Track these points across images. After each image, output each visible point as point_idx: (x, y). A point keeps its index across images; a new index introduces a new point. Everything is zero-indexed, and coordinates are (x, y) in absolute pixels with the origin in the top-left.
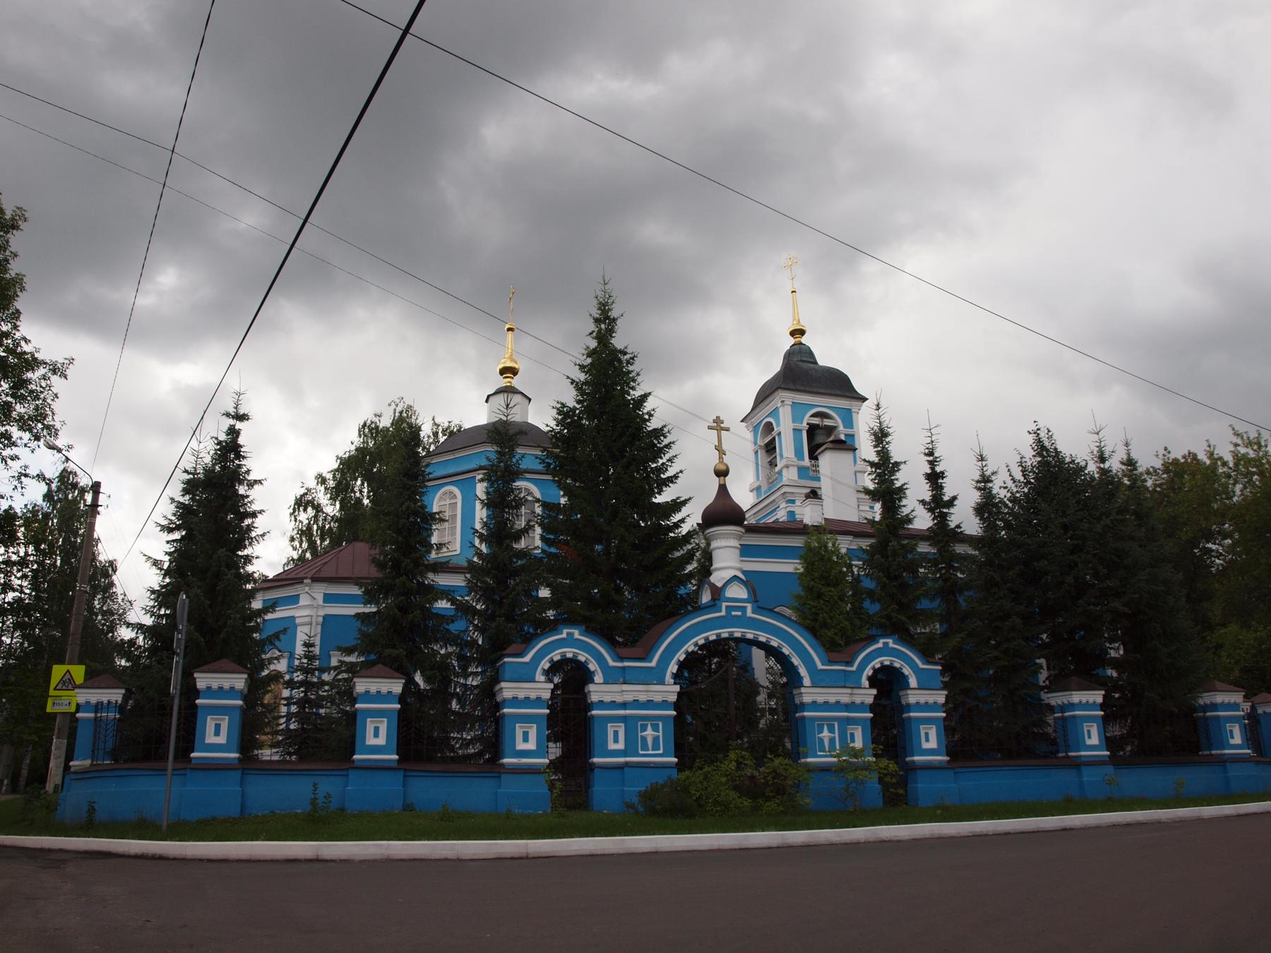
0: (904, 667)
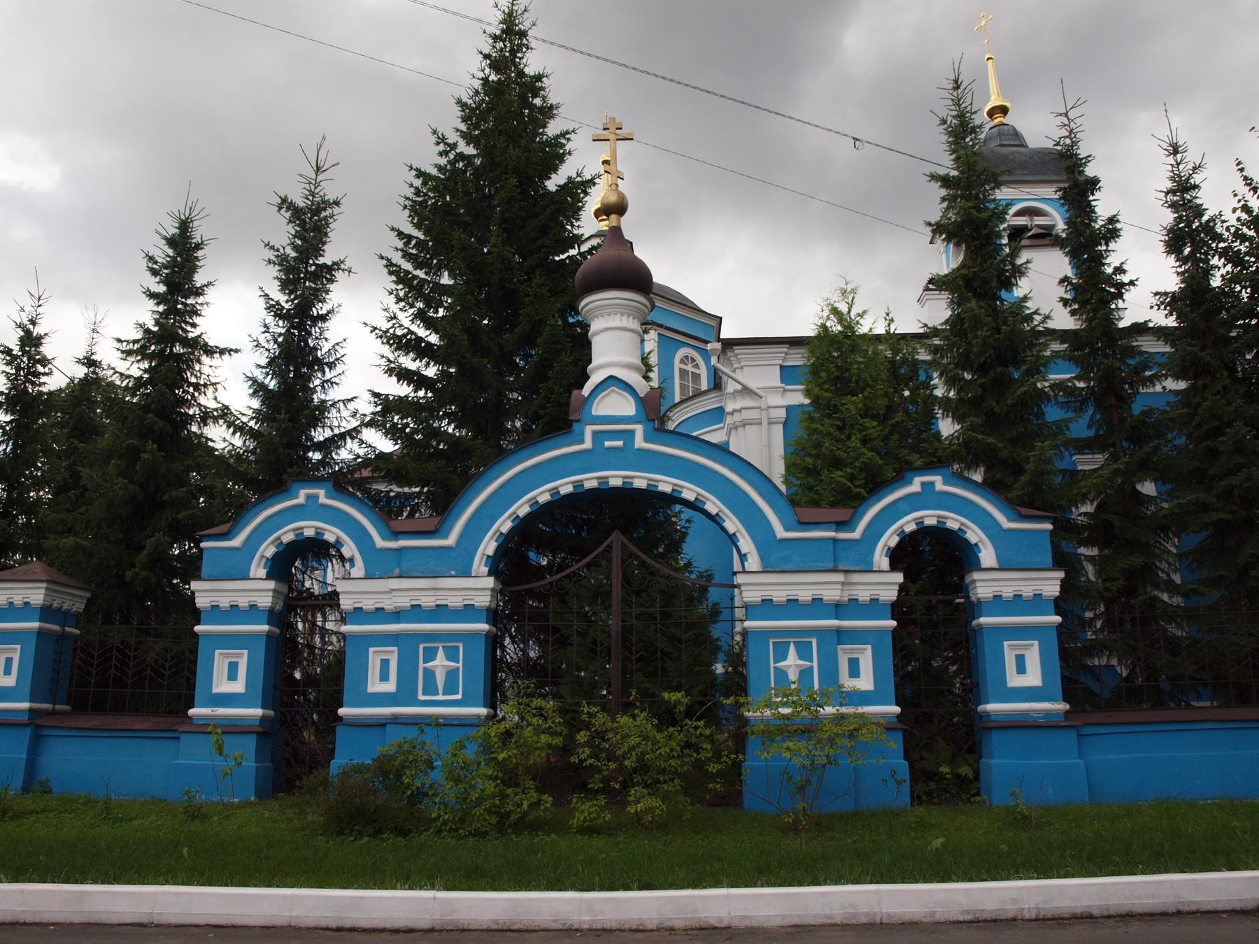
0: (968, 528)
